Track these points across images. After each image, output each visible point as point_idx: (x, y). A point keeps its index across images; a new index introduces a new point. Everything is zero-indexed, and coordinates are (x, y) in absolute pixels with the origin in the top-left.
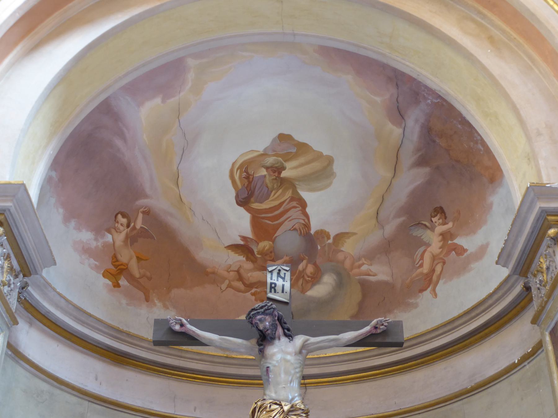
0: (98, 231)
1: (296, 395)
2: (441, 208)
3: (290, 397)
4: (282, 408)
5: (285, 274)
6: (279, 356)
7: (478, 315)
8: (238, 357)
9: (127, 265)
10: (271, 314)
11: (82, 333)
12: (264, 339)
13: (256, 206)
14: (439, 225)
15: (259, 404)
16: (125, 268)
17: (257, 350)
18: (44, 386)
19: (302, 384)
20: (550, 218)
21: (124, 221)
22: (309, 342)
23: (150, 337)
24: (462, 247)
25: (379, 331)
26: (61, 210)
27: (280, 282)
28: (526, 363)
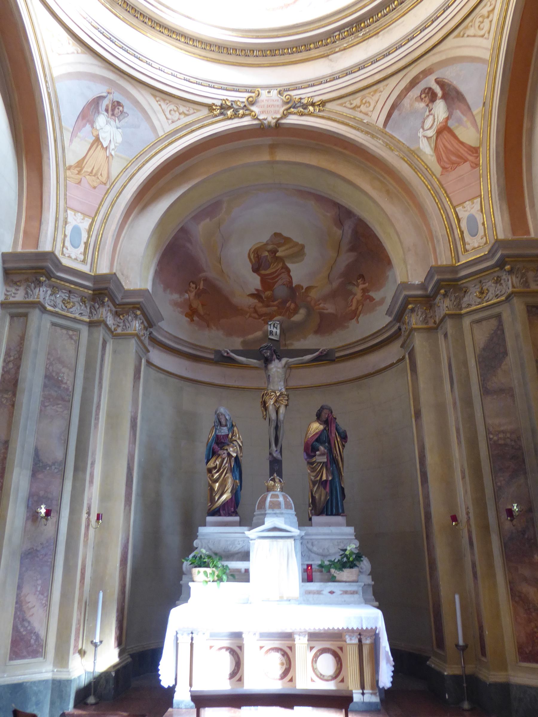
2: (362, 275)
7: (378, 336)
10: (270, 349)
11: (178, 349)
12: (267, 361)
13: (263, 272)
18: (162, 376)
20: (409, 299)
21: (194, 286)
24: (373, 297)
26: (162, 285)
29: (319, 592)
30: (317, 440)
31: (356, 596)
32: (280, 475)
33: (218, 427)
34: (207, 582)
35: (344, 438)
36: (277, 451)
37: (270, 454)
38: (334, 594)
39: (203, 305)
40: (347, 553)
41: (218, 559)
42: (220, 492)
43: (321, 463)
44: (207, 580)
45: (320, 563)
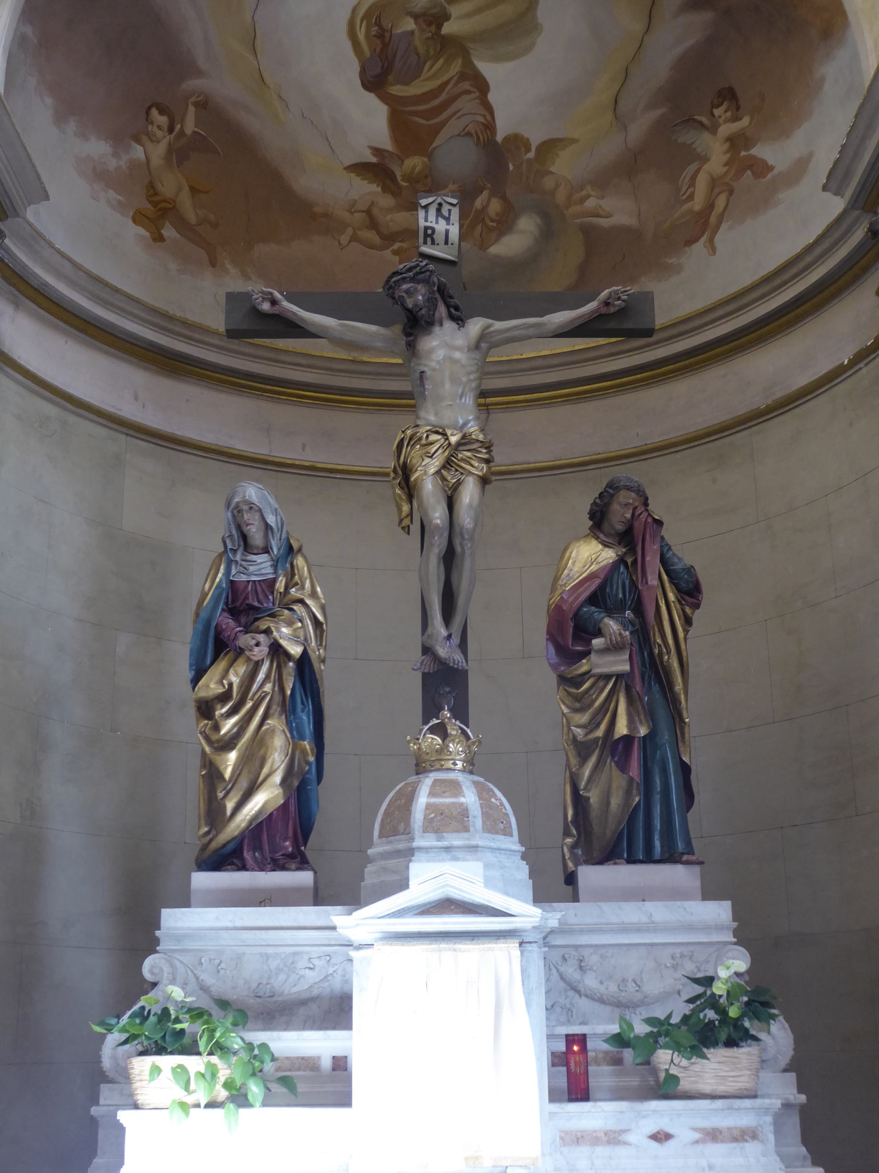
0: (119, 139)
1: (471, 418)
3: (461, 421)
4: (447, 439)
5: (450, 211)
6: (440, 354)
7: (785, 283)
8: (373, 360)
9: (174, 201)
10: (427, 282)
12: (416, 325)
13: (397, 90)
14: (726, 121)
15: (409, 432)
16: (170, 206)
17: (403, 343)
18: (50, 410)
19: (479, 405)
21: (163, 120)
22: (491, 329)
23: (222, 329)
24: (765, 162)
25: (612, 310)
26: (49, 101)
27: (441, 224)
28: (862, 365)
29: (613, 1138)
30: (594, 599)
31: (752, 1148)
32: (461, 713)
33: (238, 557)
34: (184, 1106)
35: (690, 591)
36: (449, 637)
37: (427, 650)
38: (671, 1143)
39: (194, 190)
40: (719, 988)
41: (231, 1019)
42: (243, 784)
43: (607, 677)
44: (190, 1099)
45: (615, 1029)
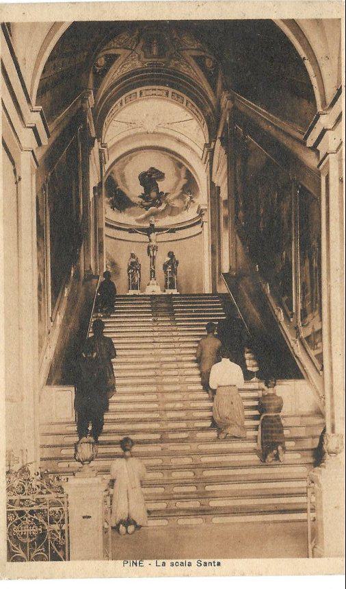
35: (177, 263)
